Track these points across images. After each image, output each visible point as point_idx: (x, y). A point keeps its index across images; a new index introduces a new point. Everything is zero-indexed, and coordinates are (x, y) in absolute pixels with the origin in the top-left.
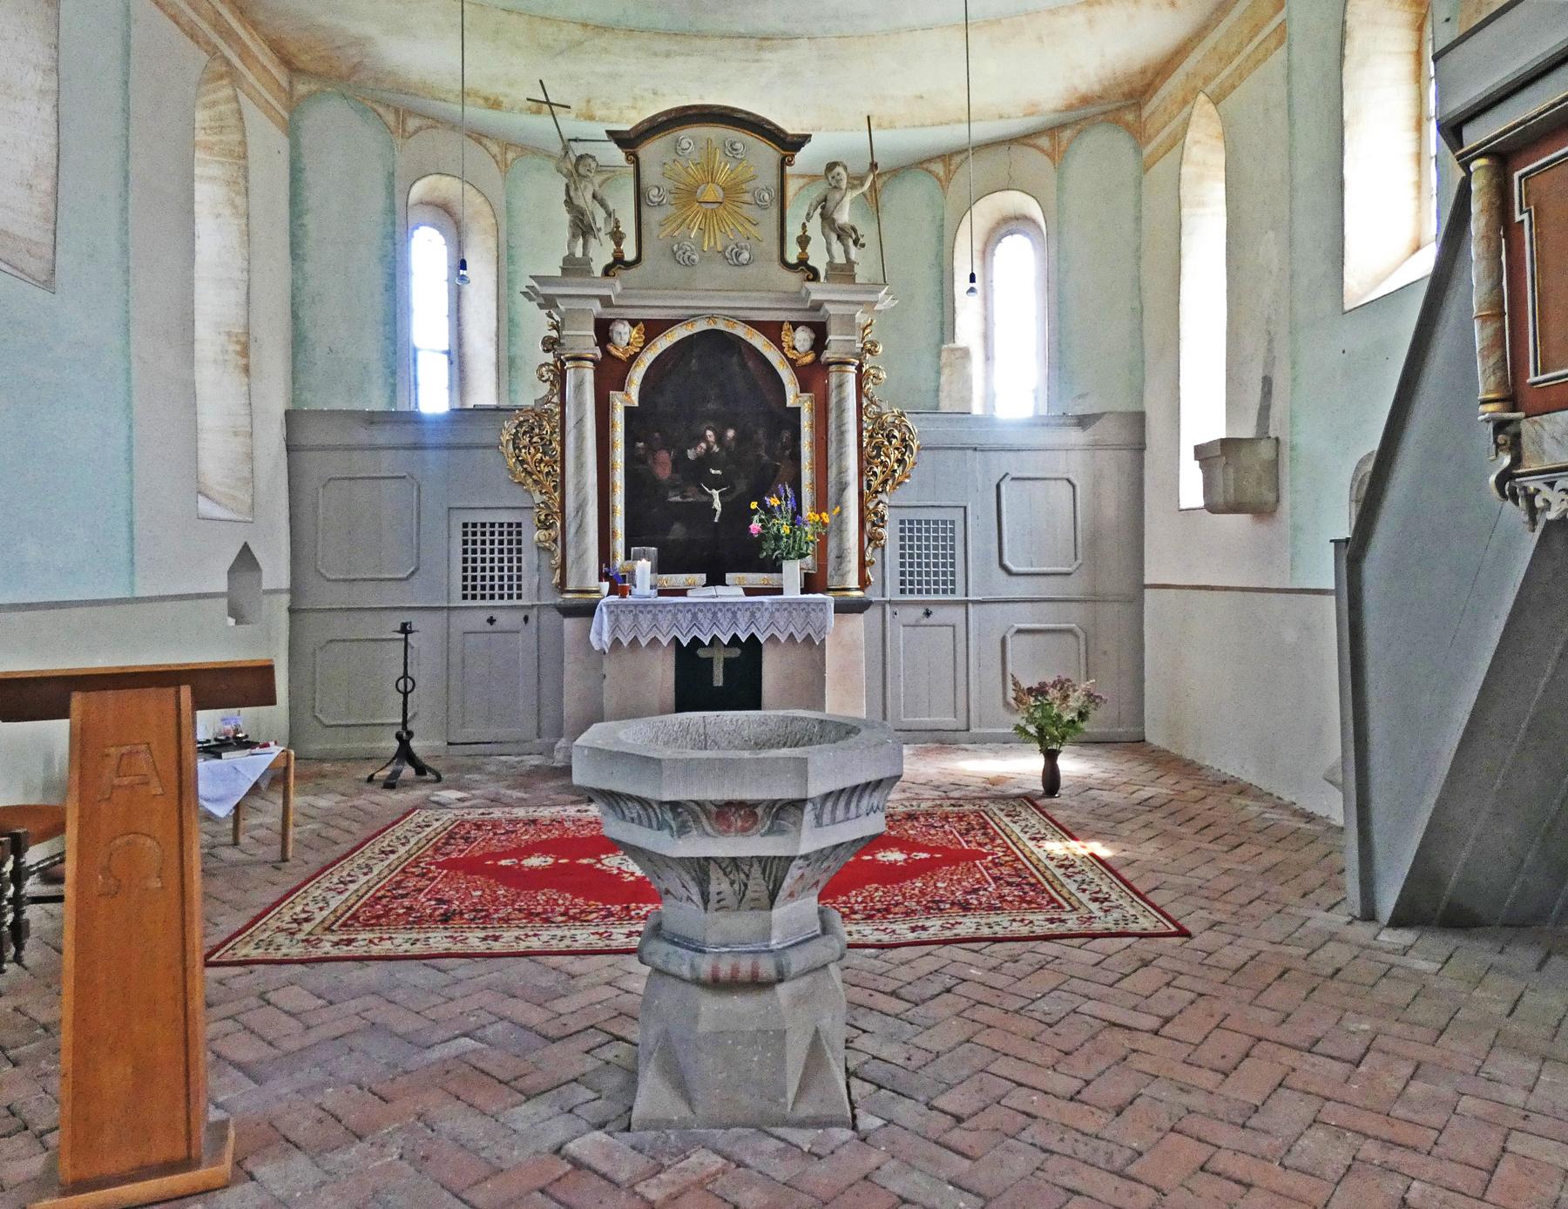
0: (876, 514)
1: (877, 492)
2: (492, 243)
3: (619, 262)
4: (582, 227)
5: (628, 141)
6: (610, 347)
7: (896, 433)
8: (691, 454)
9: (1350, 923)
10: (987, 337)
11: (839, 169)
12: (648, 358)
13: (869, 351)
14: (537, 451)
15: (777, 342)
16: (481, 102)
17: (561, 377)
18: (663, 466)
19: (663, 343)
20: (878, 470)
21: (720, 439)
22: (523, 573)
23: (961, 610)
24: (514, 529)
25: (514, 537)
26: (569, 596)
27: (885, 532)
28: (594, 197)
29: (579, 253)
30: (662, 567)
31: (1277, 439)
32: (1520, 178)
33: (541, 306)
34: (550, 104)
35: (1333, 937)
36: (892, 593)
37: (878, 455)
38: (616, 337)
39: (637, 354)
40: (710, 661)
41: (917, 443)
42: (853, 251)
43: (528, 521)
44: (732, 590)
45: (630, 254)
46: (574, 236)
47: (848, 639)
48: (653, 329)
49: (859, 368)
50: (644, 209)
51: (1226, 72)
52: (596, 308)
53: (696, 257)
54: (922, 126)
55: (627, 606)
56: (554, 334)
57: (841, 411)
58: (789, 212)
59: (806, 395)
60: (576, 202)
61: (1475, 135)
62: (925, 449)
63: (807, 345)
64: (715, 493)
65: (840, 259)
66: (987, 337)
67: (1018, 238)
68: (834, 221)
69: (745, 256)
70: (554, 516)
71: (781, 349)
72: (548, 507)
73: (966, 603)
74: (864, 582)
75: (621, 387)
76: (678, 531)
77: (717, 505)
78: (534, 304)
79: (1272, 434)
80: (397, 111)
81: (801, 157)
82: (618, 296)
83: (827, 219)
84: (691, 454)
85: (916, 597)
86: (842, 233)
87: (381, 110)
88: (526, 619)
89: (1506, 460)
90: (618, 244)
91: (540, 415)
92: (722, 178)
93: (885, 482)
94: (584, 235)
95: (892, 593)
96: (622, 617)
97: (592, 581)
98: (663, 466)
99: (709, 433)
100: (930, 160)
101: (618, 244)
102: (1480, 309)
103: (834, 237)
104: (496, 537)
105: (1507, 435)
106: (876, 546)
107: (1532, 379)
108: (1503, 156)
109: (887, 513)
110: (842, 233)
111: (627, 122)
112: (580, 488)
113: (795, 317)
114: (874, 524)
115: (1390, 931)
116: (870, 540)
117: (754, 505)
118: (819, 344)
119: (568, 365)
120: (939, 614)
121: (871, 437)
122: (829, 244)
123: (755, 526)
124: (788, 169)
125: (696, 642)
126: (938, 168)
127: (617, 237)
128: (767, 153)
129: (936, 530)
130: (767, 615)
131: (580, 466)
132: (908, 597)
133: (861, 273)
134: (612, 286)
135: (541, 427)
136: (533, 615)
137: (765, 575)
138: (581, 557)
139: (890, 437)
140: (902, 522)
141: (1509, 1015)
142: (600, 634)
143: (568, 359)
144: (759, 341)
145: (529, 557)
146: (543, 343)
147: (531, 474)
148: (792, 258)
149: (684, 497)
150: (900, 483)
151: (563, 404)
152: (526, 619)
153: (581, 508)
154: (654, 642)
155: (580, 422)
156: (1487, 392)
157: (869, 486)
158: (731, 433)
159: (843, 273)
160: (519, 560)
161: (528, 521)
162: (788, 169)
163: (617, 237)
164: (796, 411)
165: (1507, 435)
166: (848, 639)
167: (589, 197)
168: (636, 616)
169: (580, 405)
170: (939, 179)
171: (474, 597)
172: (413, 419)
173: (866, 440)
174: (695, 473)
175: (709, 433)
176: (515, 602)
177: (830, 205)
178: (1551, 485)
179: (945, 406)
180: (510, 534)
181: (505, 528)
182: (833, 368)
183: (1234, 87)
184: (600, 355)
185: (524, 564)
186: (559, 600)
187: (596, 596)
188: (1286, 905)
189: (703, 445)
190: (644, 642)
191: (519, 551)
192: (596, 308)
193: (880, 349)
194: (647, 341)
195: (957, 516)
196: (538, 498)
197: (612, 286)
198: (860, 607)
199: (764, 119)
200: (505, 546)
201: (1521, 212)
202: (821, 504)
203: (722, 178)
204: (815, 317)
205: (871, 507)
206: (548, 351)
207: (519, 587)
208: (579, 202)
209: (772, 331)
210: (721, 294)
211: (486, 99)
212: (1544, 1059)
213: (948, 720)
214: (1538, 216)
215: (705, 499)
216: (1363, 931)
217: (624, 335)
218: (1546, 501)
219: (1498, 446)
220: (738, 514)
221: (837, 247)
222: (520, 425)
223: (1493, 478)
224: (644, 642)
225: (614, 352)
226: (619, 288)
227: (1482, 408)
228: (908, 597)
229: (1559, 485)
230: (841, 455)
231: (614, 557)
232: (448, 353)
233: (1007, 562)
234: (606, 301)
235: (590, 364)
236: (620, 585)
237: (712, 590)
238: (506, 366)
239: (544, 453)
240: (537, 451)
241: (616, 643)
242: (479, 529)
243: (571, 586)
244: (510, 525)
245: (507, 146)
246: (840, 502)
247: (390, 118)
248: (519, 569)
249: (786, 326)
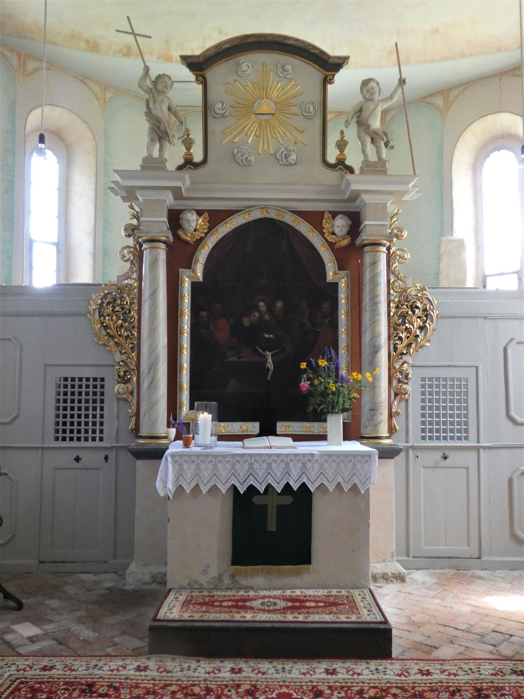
0: (401, 373)
1: (402, 354)
2: (93, 161)
4: (159, 133)
5: (198, 65)
6: (180, 233)
7: (419, 304)
8: (246, 322)
10: (477, 231)
11: (373, 84)
13: (397, 236)
14: (118, 318)
15: (320, 229)
16: (83, 45)
18: (222, 331)
19: (225, 229)
20: (403, 335)
21: (270, 308)
22: (104, 420)
23: (473, 455)
24: (98, 383)
25: (98, 389)
26: (141, 441)
27: (408, 387)
28: (169, 109)
29: (156, 154)
33: (125, 199)
34: (133, 33)
36: (415, 440)
37: (404, 323)
38: (186, 225)
39: (202, 239)
40: (264, 507)
41: (436, 312)
42: (384, 152)
44: (279, 445)
45: (198, 157)
46: (152, 140)
48: (216, 217)
49: (389, 249)
50: (210, 119)
52: (169, 199)
53: (252, 159)
54: (432, 61)
55: (189, 456)
56: (135, 222)
57: (374, 284)
58: (330, 125)
59: (343, 273)
60: (154, 112)
62: (442, 317)
63: (345, 230)
64: (269, 354)
65: (373, 157)
66: (477, 231)
67: (504, 153)
68: (369, 126)
69: (293, 157)
70: (130, 373)
71: (323, 234)
72: (126, 364)
73: (478, 449)
74: (392, 430)
75: (189, 265)
76: (234, 386)
77: (270, 364)
78: (119, 198)
80: (19, 55)
81: (340, 76)
82: (188, 190)
84: (246, 322)
85: (435, 443)
87: (7, 54)
88: (106, 458)
90: (188, 148)
92: (275, 94)
93: (409, 345)
94: (160, 139)
96: (185, 466)
97: (162, 428)
98: (222, 331)
99: (261, 304)
100: (432, 95)
101: (188, 148)
103: (368, 140)
104: (84, 389)
106: (402, 399)
109: (410, 371)
111: (196, 49)
112: (153, 348)
113: (333, 207)
114: (399, 381)
116: (396, 395)
117: (303, 365)
119: (144, 246)
120: (454, 458)
121: (397, 307)
122: (363, 145)
123: (305, 385)
124: (329, 87)
125: (252, 489)
126: (439, 101)
127: (188, 143)
128: (308, 74)
129: (438, 386)
130: (317, 466)
131: (153, 330)
132: (428, 443)
133: (391, 168)
134: (183, 180)
135: (122, 298)
136: (112, 456)
137: (307, 424)
138: (153, 406)
139: (413, 308)
140: (423, 379)
142: (165, 482)
143: (145, 241)
144: (304, 228)
145: (110, 407)
146: (126, 230)
147: (112, 337)
148: (332, 158)
149: (240, 357)
150: (422, 347)
151: (140, 279)
152: (106, 458)
154: (214, 489)
155: (154, 293)
157: (395, 349)
158: (279, 304)
159: (376, 168)
160: (102, 409)
161: (110, 376)
162: (329, 87)
163: (188, 143)
164: (335, 286)
167: (165, 110)
168: (198, 465)
169: (154, 279)
170: (439, 109)
171: (64, 439)
173: (393, 310)
174: (250, 337)
175: (261, 304)
176: (98, 444)
177: (365, 114)
179: (444, 283)
180: (95, 387)
181: (91, 383)
182: (367, 249)
184: (171, 239)
185: (106, 412)
186: (132, 445)
187: (165, 441)
189: (257, 314)
190: (204, 489)
191: (102, 401)
192: (169, 199)
193: (405, 234)
194: (210, 228)
195: (470, 374)
196: (118, 357)
197: (183, 180)
199: (309, 45)
200: (91, 397)
203: (275, 94)
204: (352, 207)
205: (397, 367)
206: (129, 236)
207: (101, 431)
208: (157, 112)
209: (315, 218)
210: (271, 184)
211: (87, 42)
213: (460, 548)
215: (257, 359)
217: (193, 222)
220: (289, 372)
221: (370, 148)
222: (105, 296)
224: (204, 489)
225: (183, 236)
226: (188, 183)
228: (428, 443)
230: (374, 322)
231: (181, 407)
232: (57, 244)
233: (513, 414)
234: (177, 192)
235: (163, 246)
237: (266, 441)
238: (100, 254)
239: (125, 320)
240: (118, 318)
241: (180, 489)
242: (84, 382)
243: (144, 432)
244: (95, 379)
245: (106, 87)
246: (373, 364)
247: (14, 60)
248: (102, 416)
249: (326, 215)
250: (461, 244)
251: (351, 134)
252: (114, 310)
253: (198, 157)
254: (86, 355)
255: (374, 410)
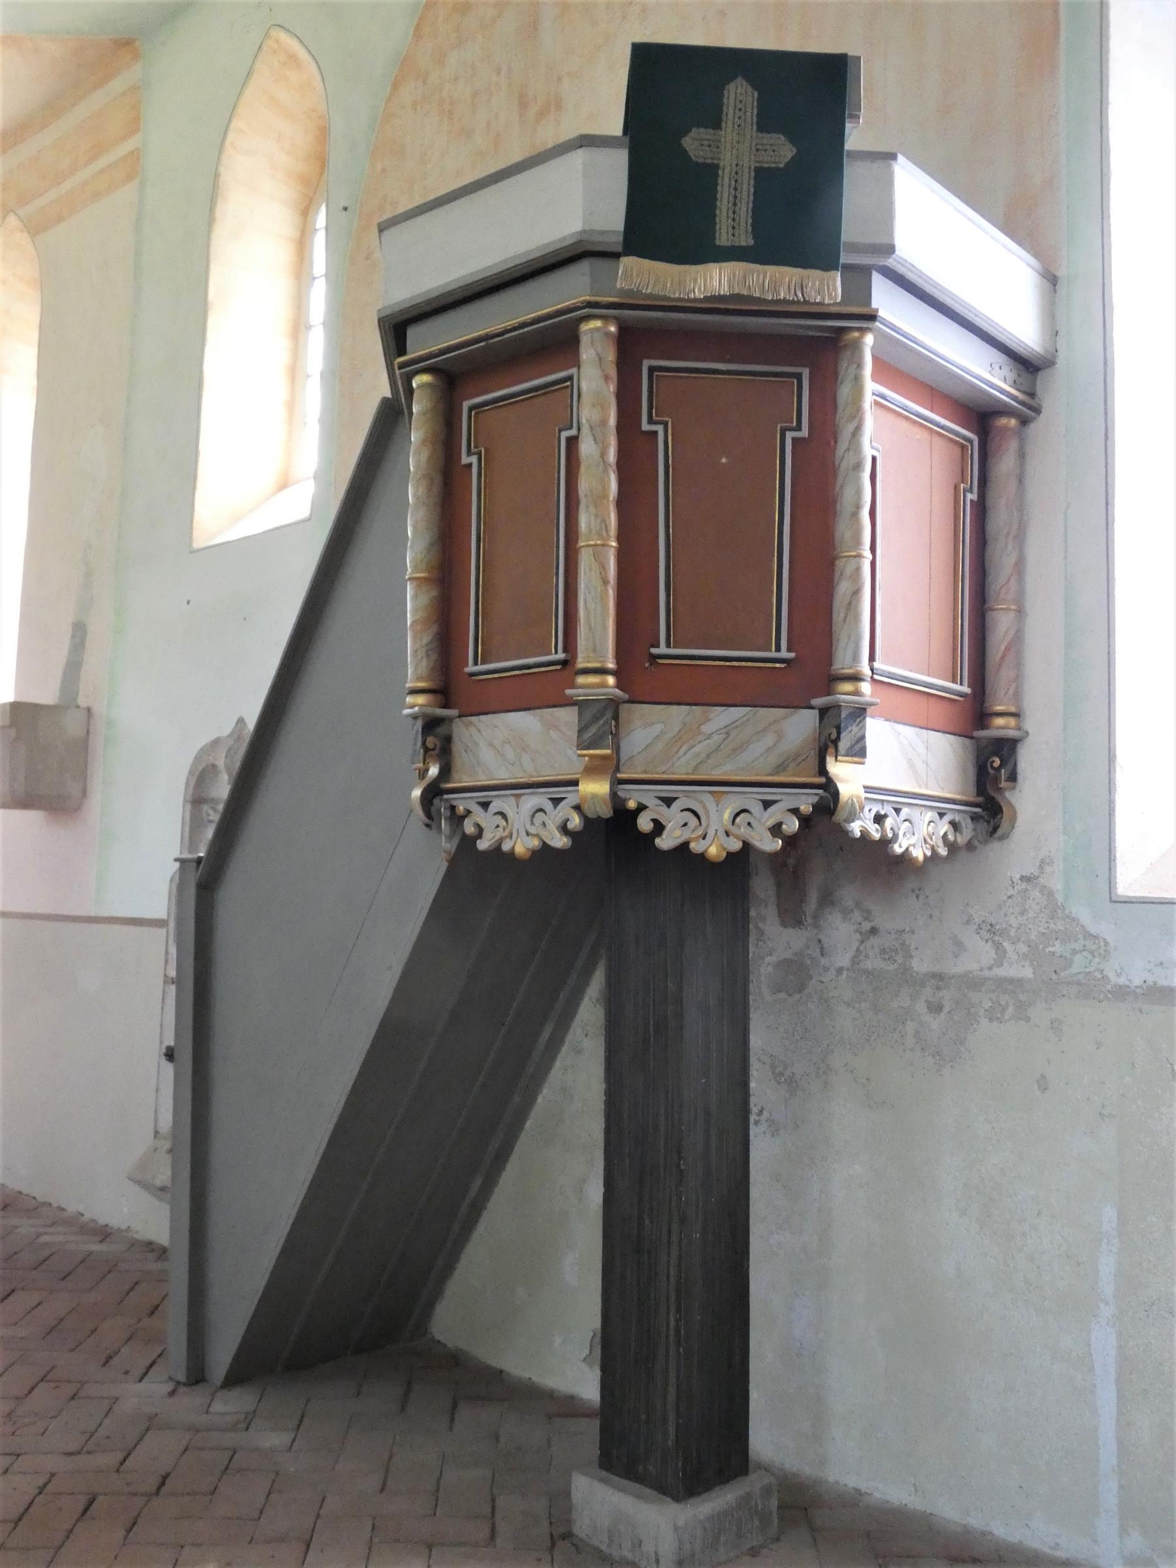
9: (172, 1393)
31: (89, 710)
32: (471, 409)
35: (152, 1423)
51: (53, 194)
61: (425, 341)
79: (82, 701)
89: (434, 771)
102: (416, 569)
105: (436, 736)
107: (471, 668)
108: (455, 376)
115: (225, 1392)
156: (419, 679)
165: (436, 736)
178: (485, 805)
183: (60, 219)
188: (83, 1384)
201: (469, 453)
212: (430, 1547)
214: (487, 461)
216: (191, 1402)
218: (478, 826)
219: (427, 750)
223: (417, 793)
227: (409, 699)
229: (493, 807)
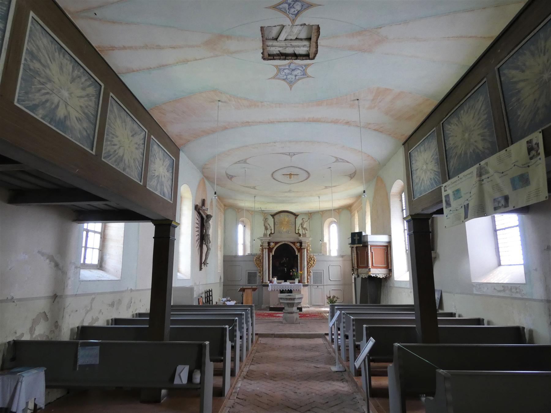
3: (271, 233)
4: (266, 229)
10: (329, 241)
12: (275, 248)
15: (295, 245)
17: (263, 251)
30: (278, 279)
43: (258, 272)
44: (288, 283)
45: (273, 232)
47: (305, 291)
48: (276, 243)
66: (329, 241)
74: (308, 282)
75: (271, 252)
83: (302, 227)
86: (304, 229)
91: (259, 256)
95: (312, 283)
110: (304, 229)
118: (301, 245)
127: (271, 230)
131: (266, 264)
141: (78, 97)
144: (292, 245)
145: (258, 278)
153: (266, 270)
161: (258, 272)
163: (271, 230)
166: (305, 291)
172: (236, 256)
198: (307, 285)
202: (301, 270)
209: (294, 243)
213: (321, 304)
217: (272, 244)
220: (289, 272)
236: (271, 282)
238: (252, 246)
246: (304, 270)
250: (326, 243)
251: (300, 228)
252: (259, 260)
253: (273, 232)
254: (252, 267)
255: (304, 278)
